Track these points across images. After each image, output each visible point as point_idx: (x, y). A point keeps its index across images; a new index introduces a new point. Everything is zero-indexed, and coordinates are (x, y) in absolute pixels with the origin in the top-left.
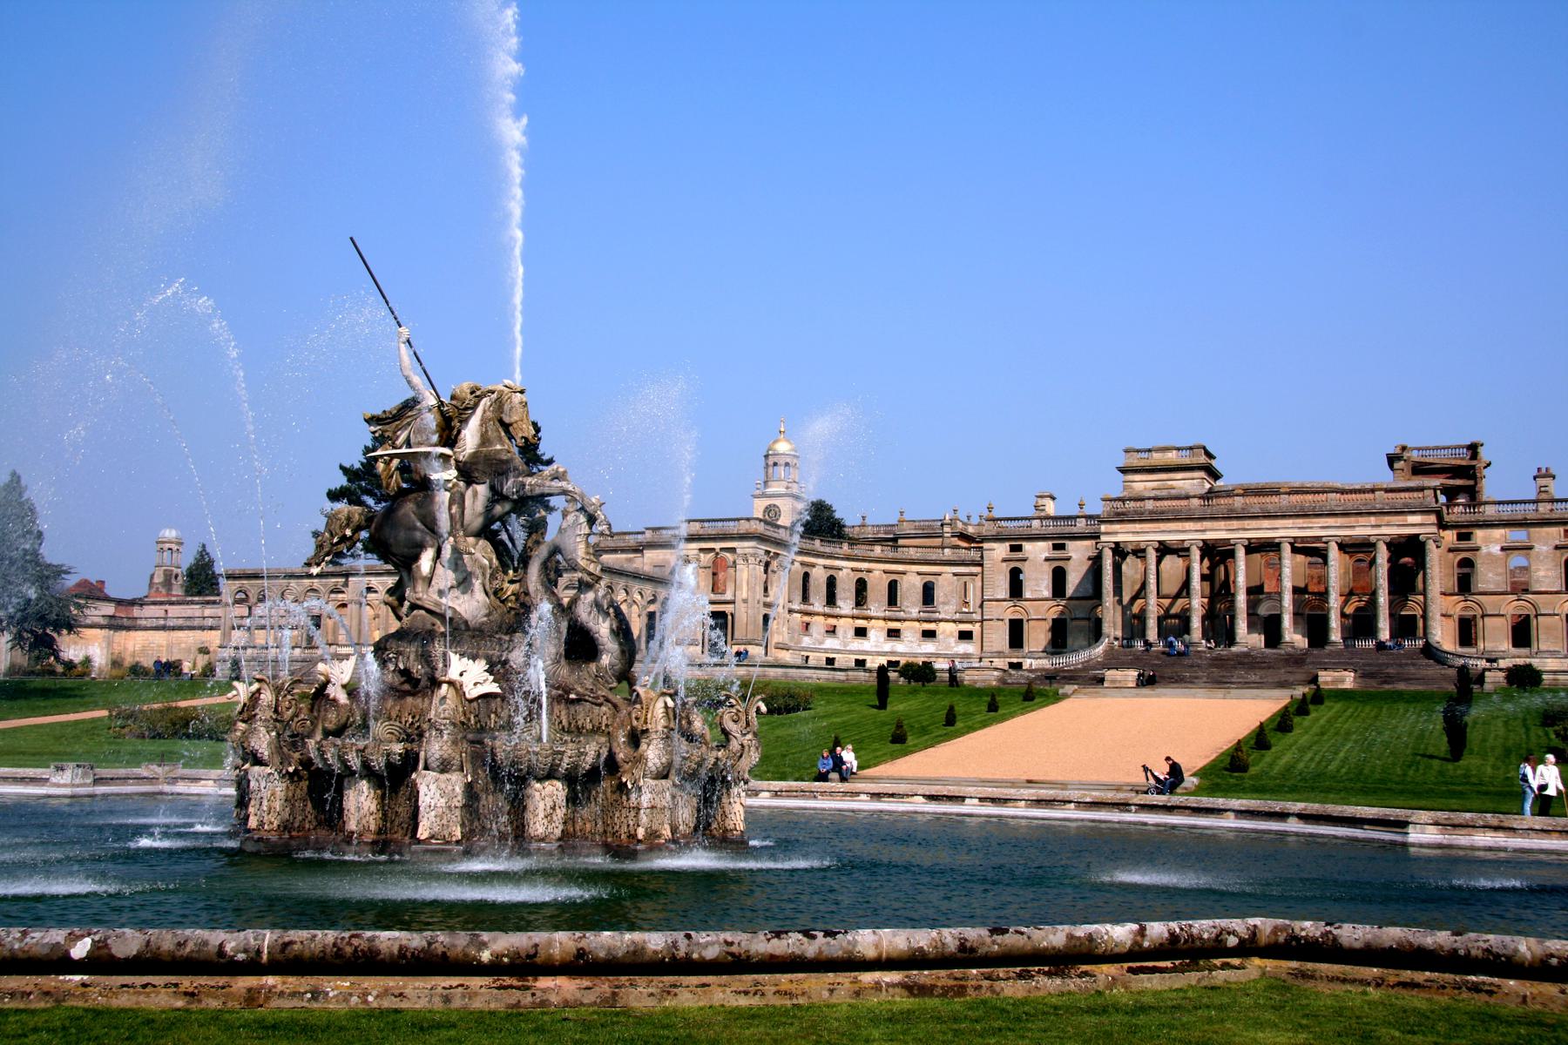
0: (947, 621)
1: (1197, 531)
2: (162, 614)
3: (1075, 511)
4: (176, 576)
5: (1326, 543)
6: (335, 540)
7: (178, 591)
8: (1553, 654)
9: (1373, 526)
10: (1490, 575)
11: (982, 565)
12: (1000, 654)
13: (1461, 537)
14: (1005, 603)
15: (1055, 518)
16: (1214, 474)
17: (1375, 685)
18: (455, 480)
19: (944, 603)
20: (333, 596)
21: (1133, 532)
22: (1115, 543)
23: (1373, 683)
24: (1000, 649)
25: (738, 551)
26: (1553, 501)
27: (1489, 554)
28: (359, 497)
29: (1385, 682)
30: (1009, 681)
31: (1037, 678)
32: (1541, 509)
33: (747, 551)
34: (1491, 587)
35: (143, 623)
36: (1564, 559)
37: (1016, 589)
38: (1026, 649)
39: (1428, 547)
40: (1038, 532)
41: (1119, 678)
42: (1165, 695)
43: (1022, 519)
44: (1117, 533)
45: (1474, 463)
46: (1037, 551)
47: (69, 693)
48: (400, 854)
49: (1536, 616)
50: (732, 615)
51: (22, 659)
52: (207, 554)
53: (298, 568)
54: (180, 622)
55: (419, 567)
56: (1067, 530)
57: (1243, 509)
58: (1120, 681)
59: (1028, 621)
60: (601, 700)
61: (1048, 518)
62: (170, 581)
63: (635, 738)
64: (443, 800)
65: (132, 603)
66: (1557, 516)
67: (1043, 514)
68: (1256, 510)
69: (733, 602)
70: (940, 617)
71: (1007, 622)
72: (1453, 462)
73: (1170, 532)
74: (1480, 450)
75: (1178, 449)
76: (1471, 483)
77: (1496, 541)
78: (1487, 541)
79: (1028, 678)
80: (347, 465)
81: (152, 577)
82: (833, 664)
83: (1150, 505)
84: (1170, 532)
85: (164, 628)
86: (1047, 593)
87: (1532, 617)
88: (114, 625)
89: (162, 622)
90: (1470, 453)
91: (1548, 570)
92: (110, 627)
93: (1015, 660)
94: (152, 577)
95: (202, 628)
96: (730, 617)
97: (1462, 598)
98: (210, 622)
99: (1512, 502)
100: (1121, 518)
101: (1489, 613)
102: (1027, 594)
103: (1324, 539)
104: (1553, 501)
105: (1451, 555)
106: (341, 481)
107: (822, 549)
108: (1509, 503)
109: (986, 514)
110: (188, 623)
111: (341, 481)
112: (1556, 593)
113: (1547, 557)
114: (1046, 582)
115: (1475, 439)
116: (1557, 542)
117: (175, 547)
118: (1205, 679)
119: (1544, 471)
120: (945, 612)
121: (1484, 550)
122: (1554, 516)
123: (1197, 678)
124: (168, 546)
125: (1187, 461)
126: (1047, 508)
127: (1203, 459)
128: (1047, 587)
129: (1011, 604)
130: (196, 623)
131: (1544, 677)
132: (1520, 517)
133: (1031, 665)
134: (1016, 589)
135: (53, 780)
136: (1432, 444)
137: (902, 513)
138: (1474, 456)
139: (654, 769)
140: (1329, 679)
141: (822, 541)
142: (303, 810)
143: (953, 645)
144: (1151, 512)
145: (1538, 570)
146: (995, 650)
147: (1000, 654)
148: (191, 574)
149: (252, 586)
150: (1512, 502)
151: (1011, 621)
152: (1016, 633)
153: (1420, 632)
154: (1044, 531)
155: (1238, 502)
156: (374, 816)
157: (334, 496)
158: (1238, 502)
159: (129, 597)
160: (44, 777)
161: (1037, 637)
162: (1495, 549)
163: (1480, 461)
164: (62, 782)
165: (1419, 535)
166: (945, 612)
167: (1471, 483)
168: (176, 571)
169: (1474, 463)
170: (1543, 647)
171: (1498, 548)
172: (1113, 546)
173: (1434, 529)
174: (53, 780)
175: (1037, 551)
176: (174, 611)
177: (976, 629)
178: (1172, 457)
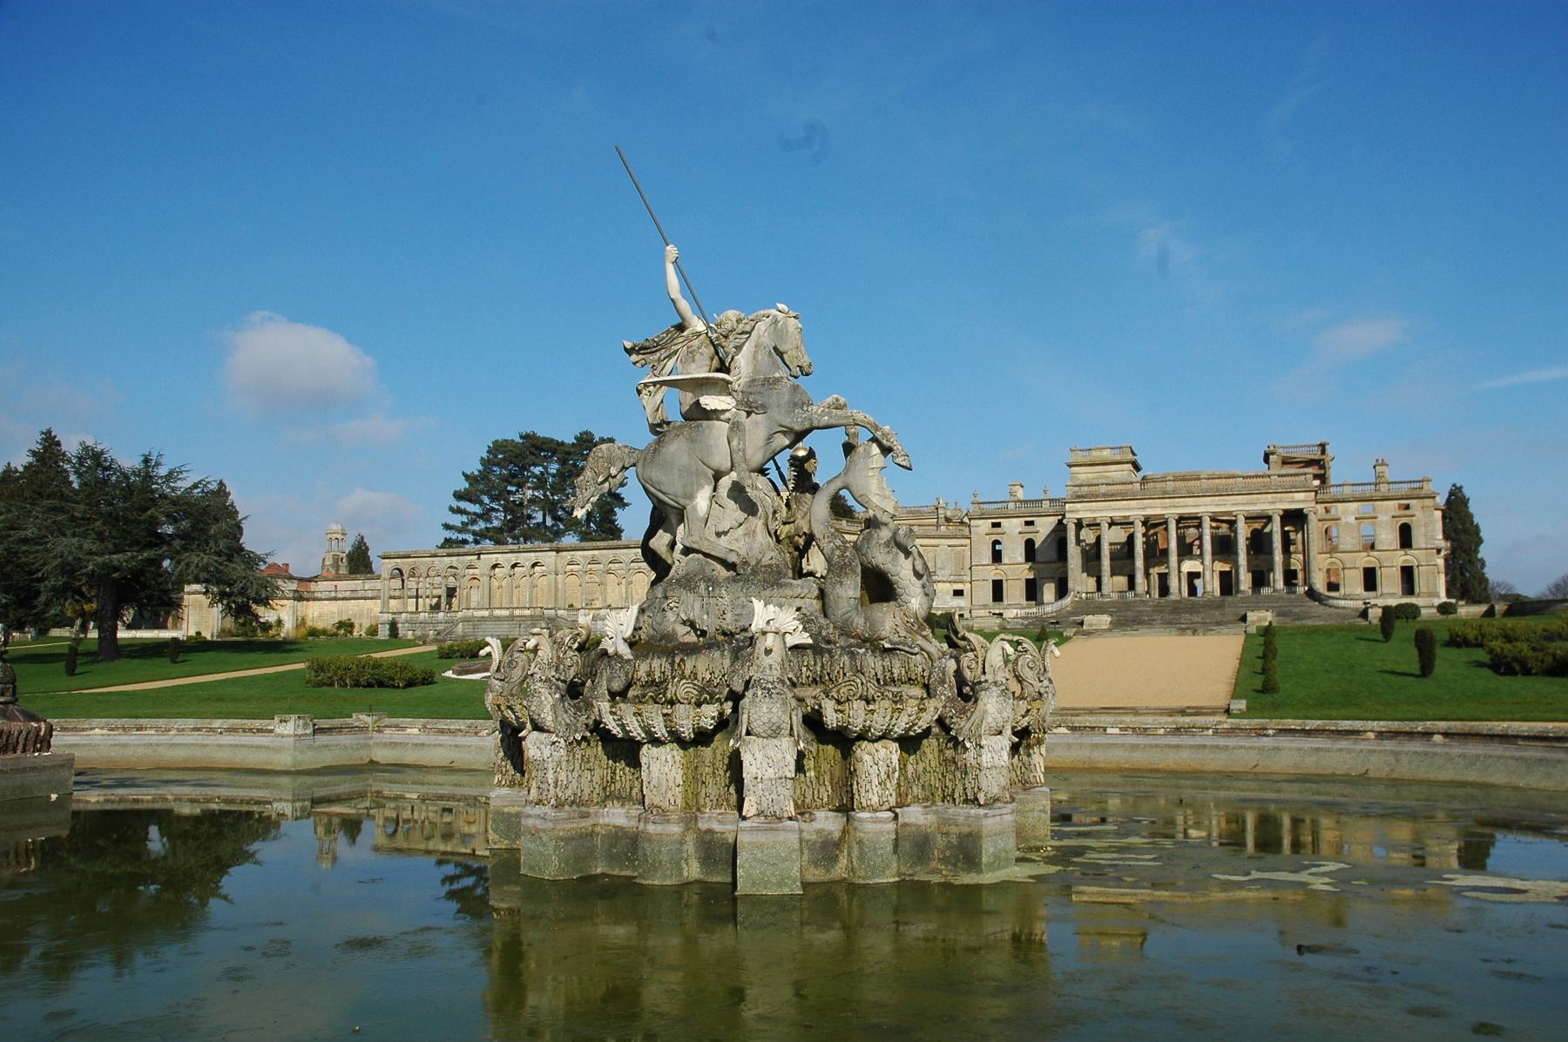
0: (944, 582)
1: (1138, 508)
2: (333, 588)
4: (342, 559)
5: (1235, 516)
6: (600, 479)
7: (343, 571)
8: (1392, 595)
9: (1270, 503)
10: (1348, 538)
11: (970, 538)
12: (985, 607)
13: (1327, 511)
15: (1026, 502)
16: (1137, 468)
17: (1288, 621)
18: (734, 410)
19: (941, 569)
20: (449, 570)
21: (1091, 510)
22: (1078, 519)
23: (1287, 620)
24: (986, 603)
26: (1389, 483)
27: (1347, 523)
28: (479, 497)
29: (1296, 619)
30: (1008, 627)
31: (1030, 624)
32: (1382, 489)
34: (1349, 548)
35: (319, 595)
36: (1399, 525)
37: (997, 557)
38: (1005, 602)
39: (1309, 518)
42: (1108, 637)
44: (1078, 511)
45: (1323, 457)
46: (1013, 526)
47: (288, 647)
48: (686, 817)
49: (1380, 568)
50: (1111, 544)
51: (229, 622)
52: (365, 544)
53: (433, 550)
54: (348, 594)
55: (695, 508)
56: (1035, 510)
57: (1173, 491)
58: (1096, 625)
60: (917, 650)
61: (1020, 501)
62: (338, 563)
63: (967, 692)
64: (771, 771)
65: (310, 580)
66: (1393, 494)
67: (1015, 499)
70: (939, 579)
71: (1362, 569)
72: (1310, 457)
73: (1119, 509)
74: (1327, 447)
76: (1323, 472)
77: (1352, 514)
78: (1346, 512)
79: (1022, 624)
80: (468, 472)
81: (324, 560)
84: (1119, 509)
85: (336, 599)
86: (1021, 559)
87: (1377, 569)
88: (299, 597)
89: (333, 594)
90: (1320, 448)
91: (1388, 533)
92: (295, 599)
93: (997, 612)
94: (324, 560)
95: (365, 599)
97: (1403, 552)
98: (370, 594)
99: (1362, 484)
100: (1081, 498)
101: (1348, 566)
102: (1005, 560)
103: (1234, 513)
104: (1389, 483)
105: (1320, 523)
106: (463, 485)
107: (848, 528)
108: (1359, 485)
109: (973, 499)
110: (354, 595)
111: (463, 485)
113: (1387, 524)
114: (1020, 551)
115: (1323, 441)
116: (1394, 514)
117: (340, 537)
118: (1160, 621)
119: (1380, 461)
120: (943, 576)
121: (1343, 520)
122: (1390, 494)
123: (1153, 620)
124: (335, 536)
125: (1118, 458)
126: (1018, 495)
127: (1130, 457)
128: (1021, 555)
129: (994, 567)
130: (360, 594)
131: (1422, 612)
132: (1368, 495)
133: (1017, 614)
134: (997, 557)
135: (278, 731)
136: (1294, 444)
138: (1323, 452)
139: (994, 724)
140: (1255, 618)
141: (848, 521)
142: (591, 781)
143: (949, 600)
144: (1104, 495)
145: (1381, 534)
146: (981, 604)
147: (985, 607)
148: (351, 557)
149: (404, 564)
150: (1362, 484)
151: (994, 581)
152: (998, 589)
153: (1272, 585)
154: (1017, 512)
155: (1170, 485)
156: (680, 789)
157: (459, 496)
158: (1170, 485)
159: (307, 576)
160: (269, 728)
161: (1015, 592)
162: (1351, 519)
163: (1327, 456)
164: (286, 732)
166: (943, 576)
167: (1323, 472)
168: (342, 555)
169: (1323, 457)
170: (1385, 591)
171: (1353, 518)
172: (1076, 521)
173: (1313, 504)
174: (278, 731)
175: (1013, 526)
176: (342, 585)
177: (966, 588)
178: (1106, 454)
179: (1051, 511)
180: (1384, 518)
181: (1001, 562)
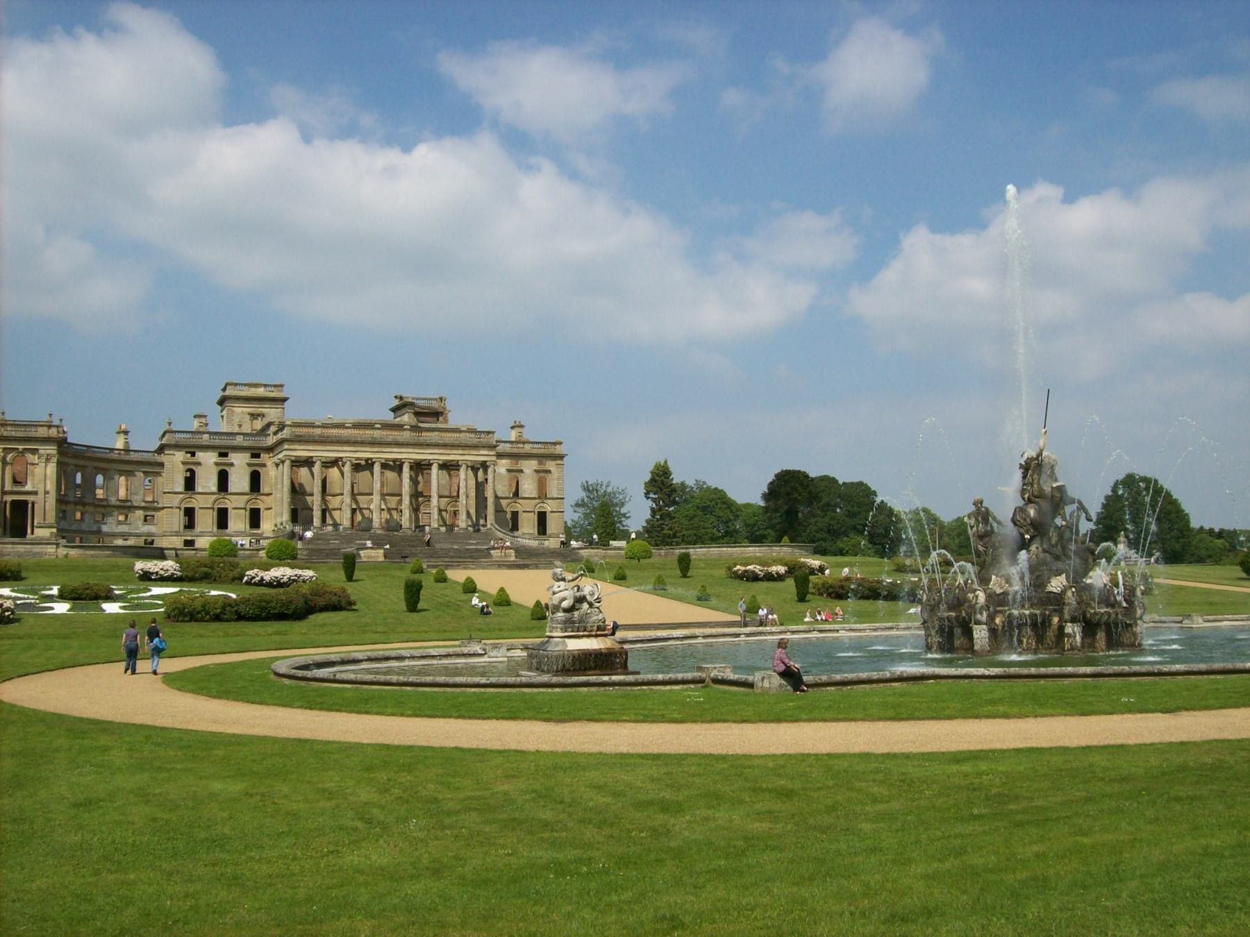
3: (236, 430)
12: (177, 534)
14: (182, 496)
25: (41, 451)
33: (49, 452)
37: (190, 483)
40: (208, 443)
41: (373, 555)
43: (184, 432)
50: (33, 504)
59: (303, 509)
68: (390, 439)
69: (36, 493)
75: (265, 386)
77: (503, 465)
82: (194, 546)
83: (318, 431)
86: (214, 489)
93: (189, 538)
96: (30, 505)
102: (199, 489)
112: (534, 498)
134: (190, 483)
136: (425, 397)
137: (170, 424)
143: (140, 525)
144: (320, 436)
165: (486, 461)
175: (208, 459)
178: (260, 392)
179: (246, 444)
180: (527, 471)
181: (194, 490)
